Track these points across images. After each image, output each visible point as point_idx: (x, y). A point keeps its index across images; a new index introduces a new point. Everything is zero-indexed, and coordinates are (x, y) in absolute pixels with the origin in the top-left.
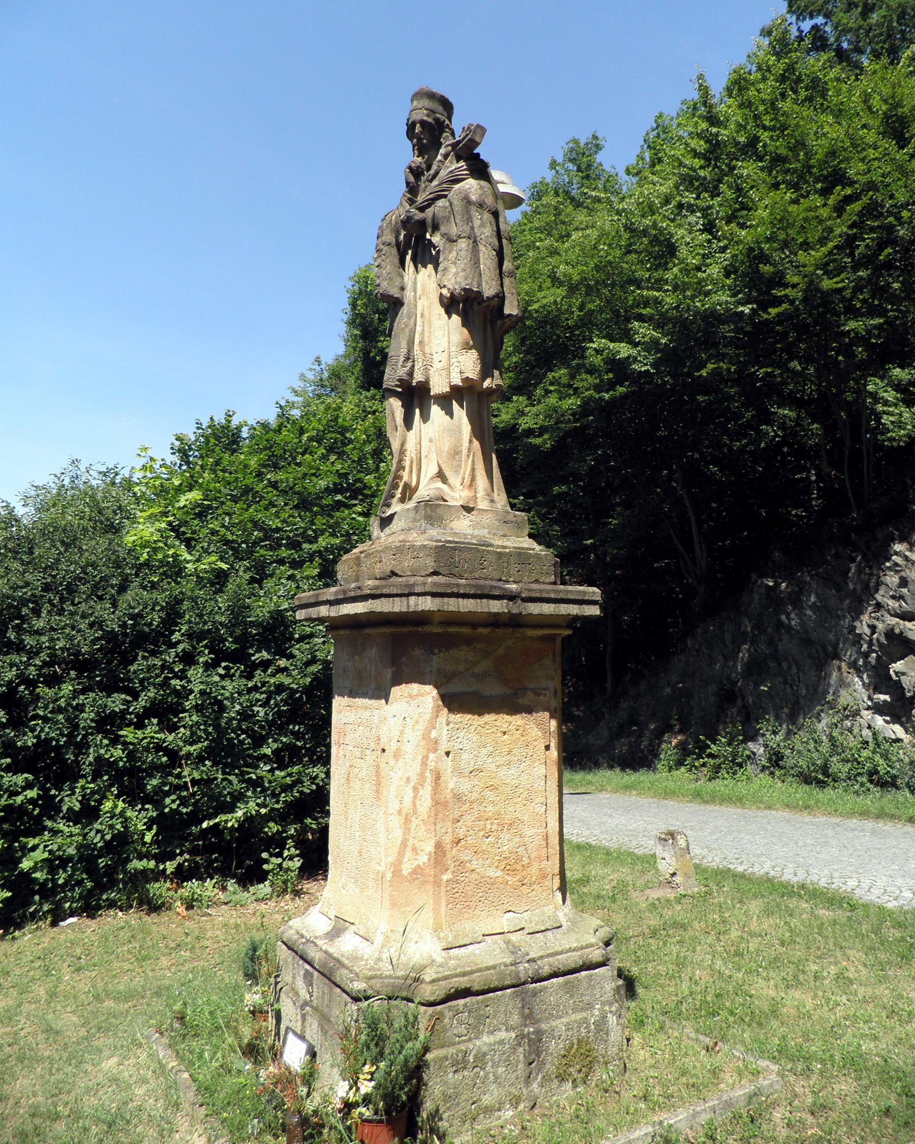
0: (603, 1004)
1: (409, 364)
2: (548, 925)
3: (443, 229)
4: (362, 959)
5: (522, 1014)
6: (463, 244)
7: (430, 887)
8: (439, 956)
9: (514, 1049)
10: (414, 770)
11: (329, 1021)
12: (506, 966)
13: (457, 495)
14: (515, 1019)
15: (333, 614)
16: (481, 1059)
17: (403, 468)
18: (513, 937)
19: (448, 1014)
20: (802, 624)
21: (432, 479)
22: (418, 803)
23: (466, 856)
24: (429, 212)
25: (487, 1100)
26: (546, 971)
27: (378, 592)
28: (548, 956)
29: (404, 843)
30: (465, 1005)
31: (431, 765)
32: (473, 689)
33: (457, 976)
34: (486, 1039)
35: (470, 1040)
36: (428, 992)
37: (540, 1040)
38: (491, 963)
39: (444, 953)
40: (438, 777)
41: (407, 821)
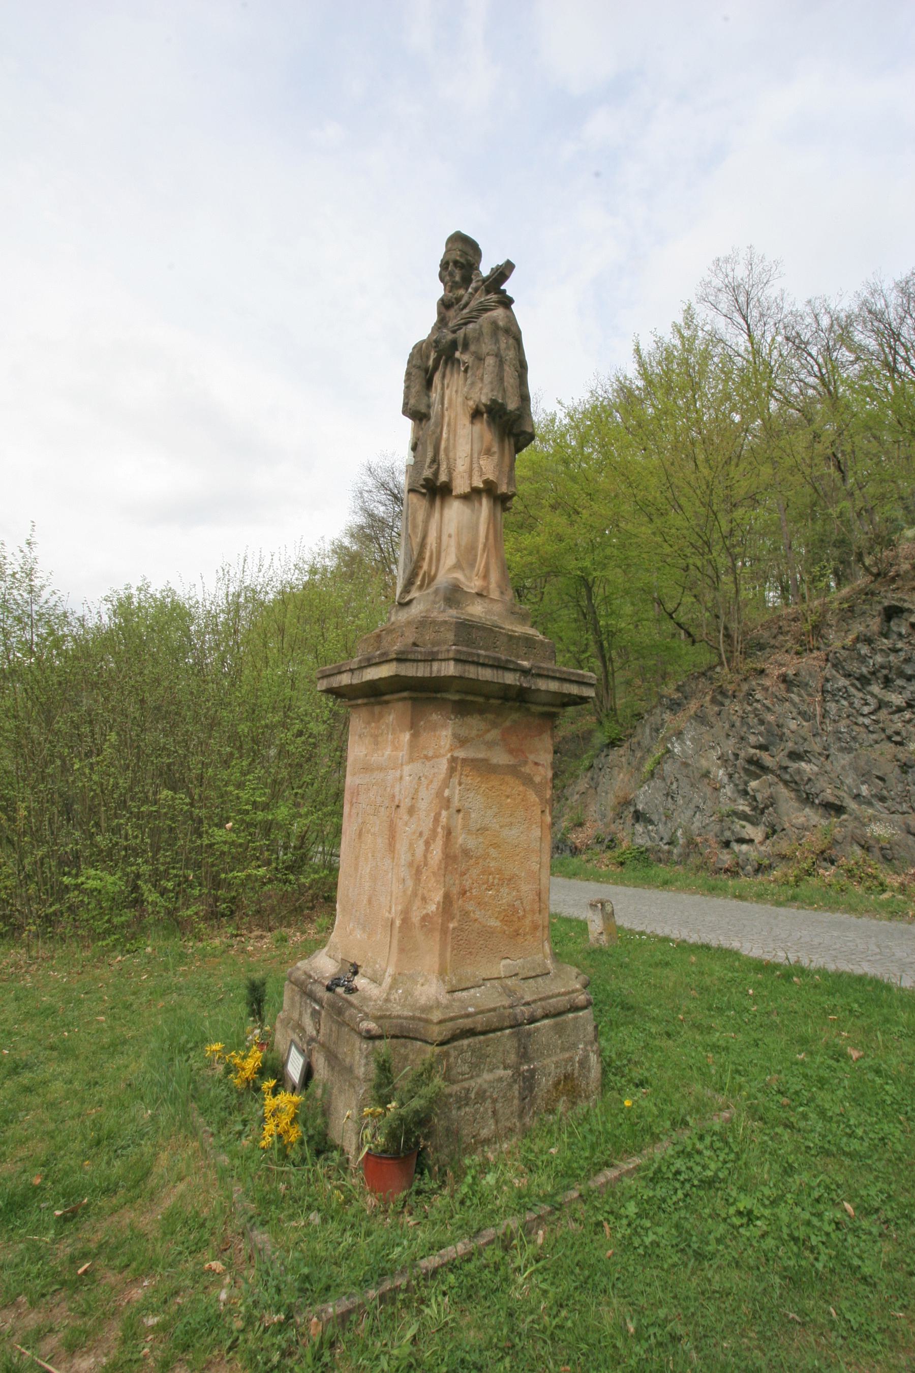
0: (586, 1044)
1: (435, 466)
2: (538, 972)
3: (472, 348)
4: (370, 999)
5: (517, 1053)
6: (490, 361)
7: (437, 936)
8: (444, 999)
9: (510, 1086)
10: (426, 825)
11: (336, 1057)
12: (504, 1008)
13: (473, 584)
14: (512, 1058)
15: (355, 681)
16: (482, 1095)
17: (424, 559)
18: (509, 982)
19: (453, 1053)
20: (683, 751)
21: (449, 569)
22: (429, 856)
23: (470, 907)
24: (461, 333)
25: (485, 1133)
26: (539, 1012)
27: (404, 657)
28: (541, 999)
29: (414, 893)
30: (469, 1046)
31: (443, 820)
32: (481, 756)
33: (461, 1017)
34: (487, 1076)
35: (472, 1077)
36: (436, 1033)
37: (533, 1077)
38: (492, 1006)
39: (448, 996)
40: (449, 833)
41: (418, 872)
